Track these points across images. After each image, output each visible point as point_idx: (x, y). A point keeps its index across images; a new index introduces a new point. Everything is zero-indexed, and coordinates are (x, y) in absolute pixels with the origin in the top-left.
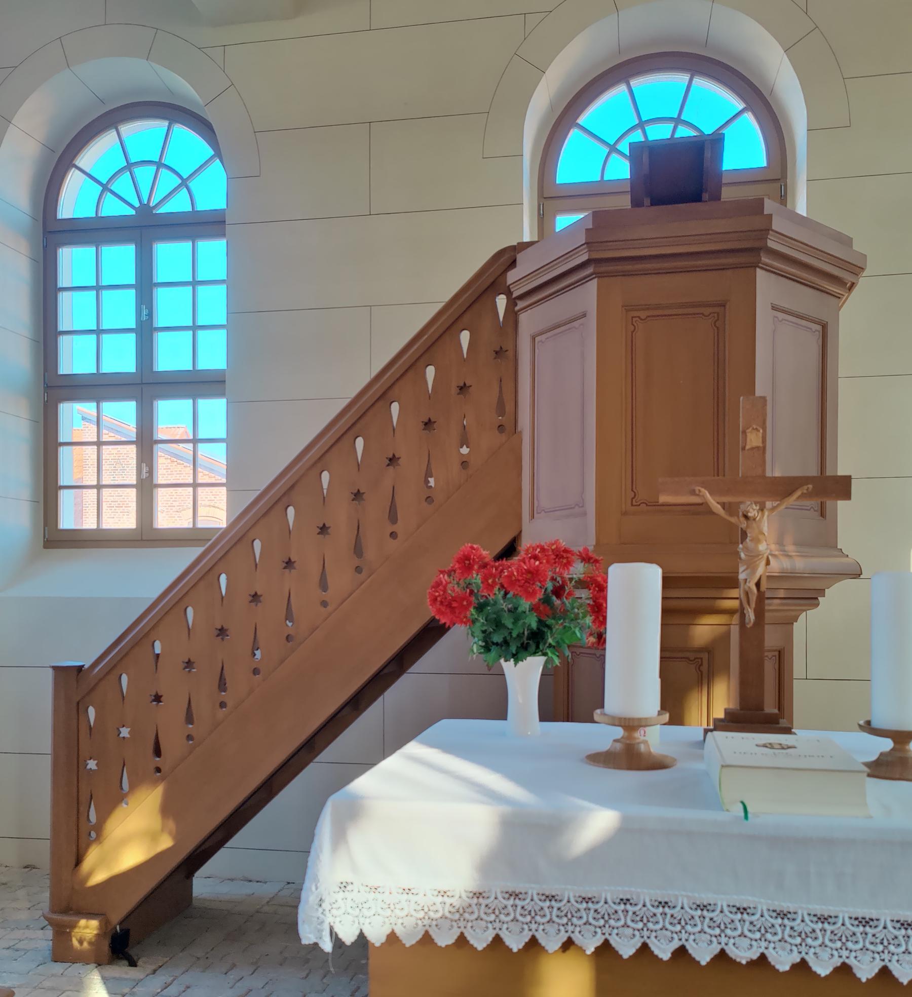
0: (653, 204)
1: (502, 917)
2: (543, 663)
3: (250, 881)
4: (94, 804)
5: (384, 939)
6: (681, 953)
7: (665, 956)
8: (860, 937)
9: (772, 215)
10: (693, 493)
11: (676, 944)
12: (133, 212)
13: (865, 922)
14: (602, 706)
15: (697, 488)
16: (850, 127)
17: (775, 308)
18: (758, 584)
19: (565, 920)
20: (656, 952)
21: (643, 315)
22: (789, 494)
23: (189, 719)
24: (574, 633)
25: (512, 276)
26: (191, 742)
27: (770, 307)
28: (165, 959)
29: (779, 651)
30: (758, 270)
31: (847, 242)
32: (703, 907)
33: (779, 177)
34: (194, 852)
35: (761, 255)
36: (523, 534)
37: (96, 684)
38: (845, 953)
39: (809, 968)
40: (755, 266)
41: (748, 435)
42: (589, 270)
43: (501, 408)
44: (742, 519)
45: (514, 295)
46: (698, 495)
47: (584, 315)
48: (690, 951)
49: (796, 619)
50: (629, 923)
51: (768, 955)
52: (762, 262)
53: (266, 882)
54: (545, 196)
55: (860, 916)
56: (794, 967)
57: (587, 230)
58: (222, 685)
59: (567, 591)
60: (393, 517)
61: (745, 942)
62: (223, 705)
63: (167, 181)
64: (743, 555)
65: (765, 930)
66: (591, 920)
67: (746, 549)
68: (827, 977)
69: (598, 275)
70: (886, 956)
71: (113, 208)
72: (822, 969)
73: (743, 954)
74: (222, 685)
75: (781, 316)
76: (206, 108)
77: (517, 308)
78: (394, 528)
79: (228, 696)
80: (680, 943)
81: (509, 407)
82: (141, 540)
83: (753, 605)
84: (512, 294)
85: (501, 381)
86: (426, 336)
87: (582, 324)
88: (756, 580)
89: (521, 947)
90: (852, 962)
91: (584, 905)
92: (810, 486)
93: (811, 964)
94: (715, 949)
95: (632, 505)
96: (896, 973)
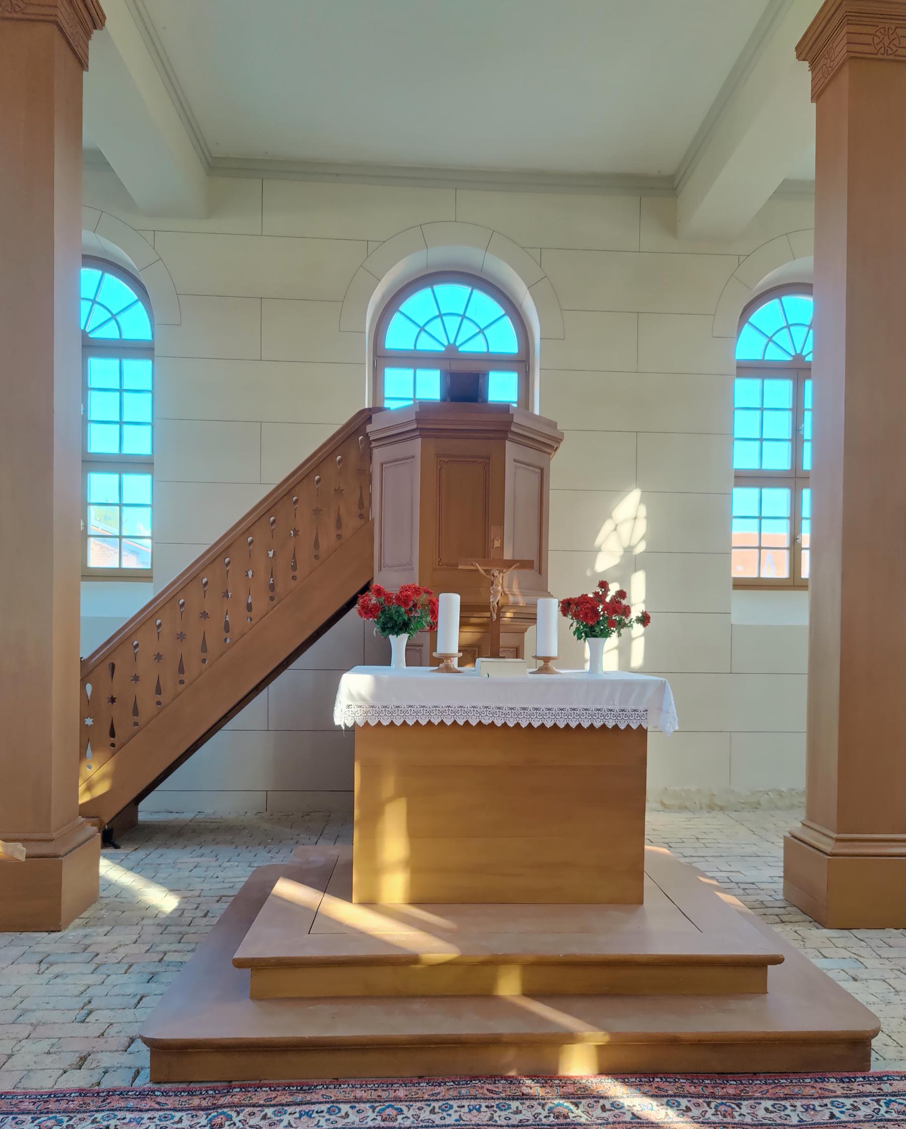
0: (452, 401)
1: (406, 714)
2: (407, 637)
3: (172, 812)
4: (91, 746)
5: (363, 724)
6: (467, 723)
7: (462, 724)
8: (522, 714)
9: (513, 414)
10: (472, 565)
11: (465, 720)
12: (443, 349)
13: (524, 709)
14: (436, 651)
15: (474, 563)
16: (564, 339)
17: (515, 461)
18: (498, 603)
19: (428, 714)
20: (459, 723)
21: (446, 460)
22: (510, 567)
23: (158, 691)
24: (423, 623)
25: (369, 428)
26: (159, 706)
27: (513, 460)
28: (138, 846)
29: (517, 648)
30: (507, 441)
31: (553, 425)
32: (474, 707)
33: (524, 360)
34: (159, 777)
35: (508, 434)
36: (374, 578)
37: (94, 669)
38: (518, 719)
39: (507, 725)
40: (506, 439)
41: (495, 542)
42: (417, 433)
43: (361, 505)
44: (492, 576)
45: (371, 439)
46: (474, 566)
47: (413, 457)
48: (470, 722)
49: (526, 630)
50: (450, 713)
51: (494, 721)
52: (508, 438)
53: (183, 813)
54: (378, 355)
55: (523, 707)
56: (502, 725)
57: (416, 412)
58: (181, 670)
59: (418, 606)
60: (294, 568)
61: (487, 718)
62: (182, 682)
63: (469, 329)
64: (492, 592)
65: (493, 714)
66: (437, 714)
67: (493, 589)
68: (513, 727)
69: (422, 437)
70: (530, 719)
72: (511, 725)
73: (486, 722)
74: (181, 670)
75: (518, 465)
76: (139, 273)
77: (371, 446)
78: (295, 573)
79: (186, 677)
80: (466, 720)
81: (366, 504)
82: (794, 586)
83: (496, 612)
84: (369, 438)
85: (361, 488)
86: (316, 458)
87: (412, 462)
88: (497, 601)
89: (413, 724)
90: (520, 722)
91: (435, 708)
92: (519, 564)
93: (507, 723)
94: (478, 720)
95: (439, 565)
96: (533, 724)
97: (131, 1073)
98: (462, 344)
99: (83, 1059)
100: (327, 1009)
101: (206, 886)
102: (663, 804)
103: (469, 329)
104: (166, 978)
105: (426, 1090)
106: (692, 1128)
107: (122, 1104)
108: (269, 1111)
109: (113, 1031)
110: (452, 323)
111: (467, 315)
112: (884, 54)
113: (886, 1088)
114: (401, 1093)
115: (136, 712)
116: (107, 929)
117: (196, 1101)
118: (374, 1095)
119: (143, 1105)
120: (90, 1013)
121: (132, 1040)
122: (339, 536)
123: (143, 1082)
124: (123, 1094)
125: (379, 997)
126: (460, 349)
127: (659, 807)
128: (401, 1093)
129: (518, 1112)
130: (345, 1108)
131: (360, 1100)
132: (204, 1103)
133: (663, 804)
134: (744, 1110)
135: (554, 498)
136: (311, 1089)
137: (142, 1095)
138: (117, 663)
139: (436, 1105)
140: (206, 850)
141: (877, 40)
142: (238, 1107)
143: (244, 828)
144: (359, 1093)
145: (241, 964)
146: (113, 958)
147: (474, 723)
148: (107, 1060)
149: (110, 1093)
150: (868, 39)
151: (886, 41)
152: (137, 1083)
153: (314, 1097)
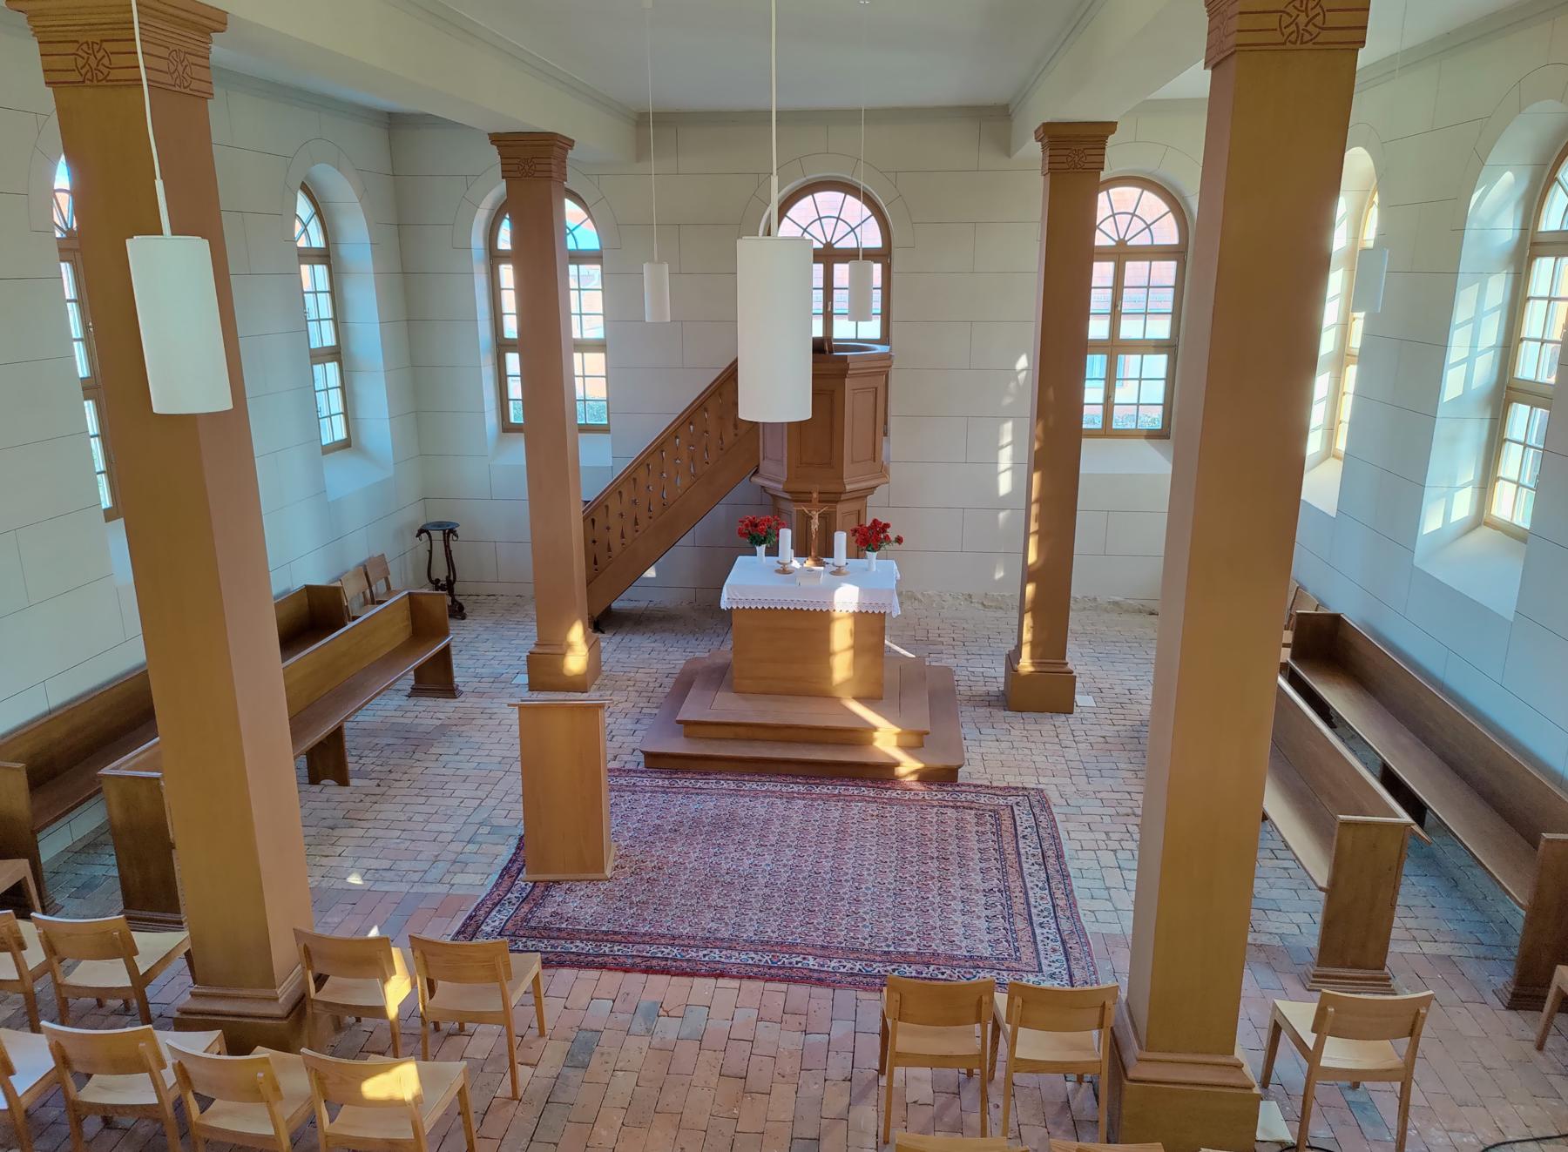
58: (636, 524)
74: (636, 524)
97: (636, 764)
98: (836, 242)
99: (616, 757)
100: (1406, 739)
101: (659, 666)
104: (645, 721)
106: (1561, 1019)
107: (635, 775)
108: (693, 781)
109: (625, 745)
110: (829, 224)
112: (1295, 43)
115: (609, 550)
116: (611, 692)
117: (664, 776)
119: (643, 775)
120: (613, 736)
121: (634, 750)
122: (736, 435)
123: (641, 767)
124: (635, 771)
126: (835, 246)
128: (746, 778)
130: (722, 782)
131: (728, 780)
132: (667, 777)
136: (710, 774)
137: (642, 772)
138: (596, 519)
139: (760, 783)
140: (657, 637)
141: (1070, 159)
142: (680, 779)
143: (681, 618)
144: (729, 777)
145: (679, 722)
146: (617, 710)
148: (626, 758)
149: (630, 770)
150: (1064, 159)
151: (1302, 19)
152: (639, 767)
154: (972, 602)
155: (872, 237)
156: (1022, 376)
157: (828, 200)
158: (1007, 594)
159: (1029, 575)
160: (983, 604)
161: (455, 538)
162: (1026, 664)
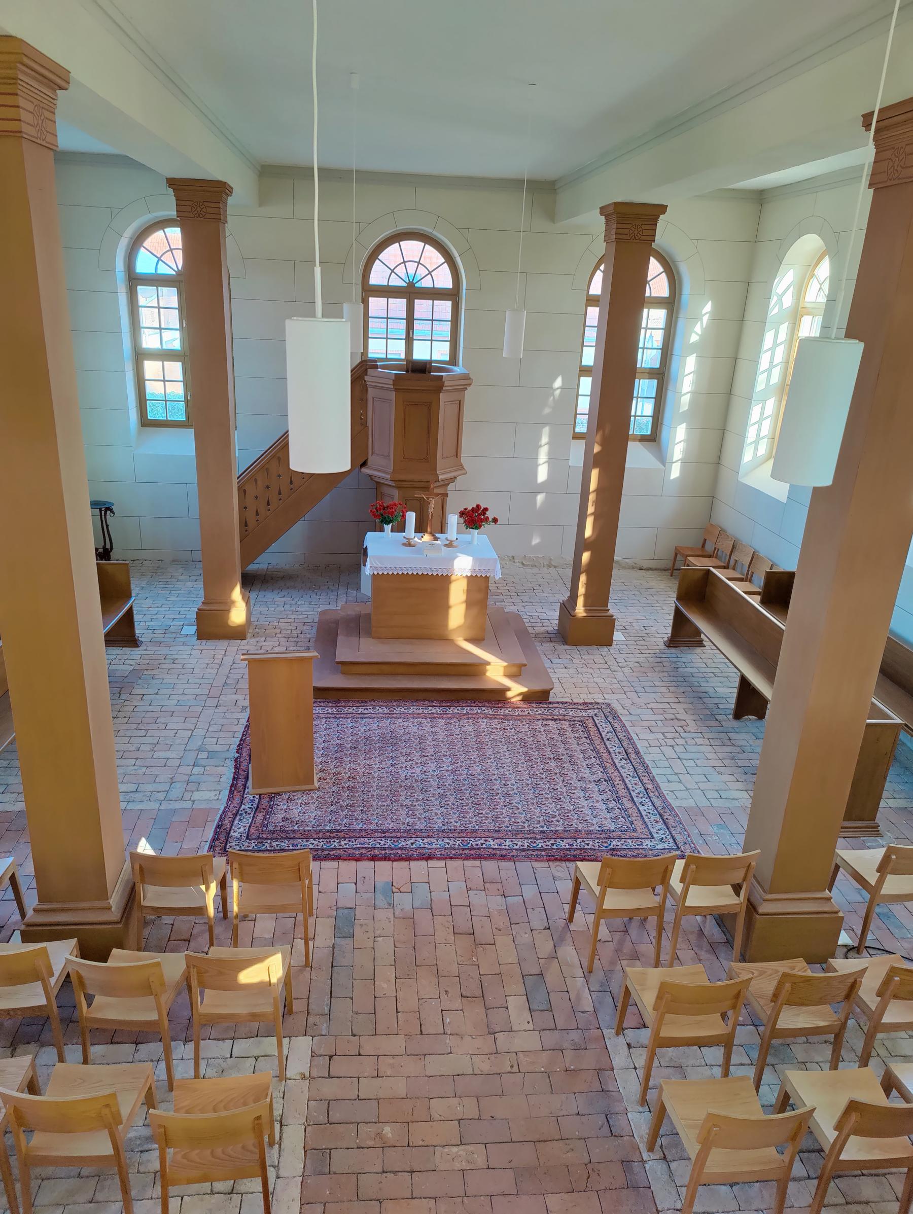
58: (268, 504)
63: (422, 271)
71: (395, 282)
73: (425, 573)
74: (268, 504)
102: (523, 564)
103: (422, 271)
105: (402, 704)
111: (421, 262)
113: (550, 706)
114: (395, 704)
118: (386, 704)
125: (384, 674)
126: (416, 285)
127: (521, 566)
129: (431, 710)
130: (378, 708)
131: (382, 706)
133: (523, 564)
134: (502, 711)
135: (466, 427)
136: (366, 702)
139: (406, 708)
141: (631, 232)
145: (338, 663)
147: (420, 574)
153: (368, 705)
154: (514, 562)
155: (444, 279)
156: (558, 392)
157: (412, 247)
158: (540, 556)
159: (582, 545)
160: (522, 563)
161: (112, 515)
162: (580, 610)
